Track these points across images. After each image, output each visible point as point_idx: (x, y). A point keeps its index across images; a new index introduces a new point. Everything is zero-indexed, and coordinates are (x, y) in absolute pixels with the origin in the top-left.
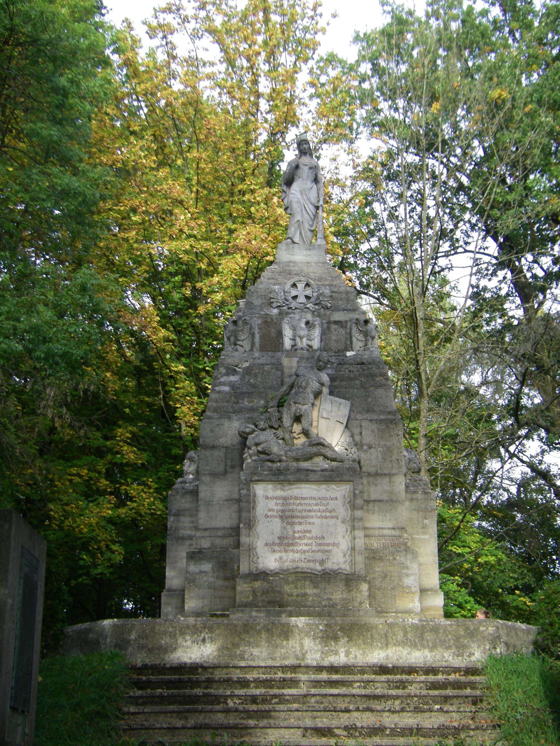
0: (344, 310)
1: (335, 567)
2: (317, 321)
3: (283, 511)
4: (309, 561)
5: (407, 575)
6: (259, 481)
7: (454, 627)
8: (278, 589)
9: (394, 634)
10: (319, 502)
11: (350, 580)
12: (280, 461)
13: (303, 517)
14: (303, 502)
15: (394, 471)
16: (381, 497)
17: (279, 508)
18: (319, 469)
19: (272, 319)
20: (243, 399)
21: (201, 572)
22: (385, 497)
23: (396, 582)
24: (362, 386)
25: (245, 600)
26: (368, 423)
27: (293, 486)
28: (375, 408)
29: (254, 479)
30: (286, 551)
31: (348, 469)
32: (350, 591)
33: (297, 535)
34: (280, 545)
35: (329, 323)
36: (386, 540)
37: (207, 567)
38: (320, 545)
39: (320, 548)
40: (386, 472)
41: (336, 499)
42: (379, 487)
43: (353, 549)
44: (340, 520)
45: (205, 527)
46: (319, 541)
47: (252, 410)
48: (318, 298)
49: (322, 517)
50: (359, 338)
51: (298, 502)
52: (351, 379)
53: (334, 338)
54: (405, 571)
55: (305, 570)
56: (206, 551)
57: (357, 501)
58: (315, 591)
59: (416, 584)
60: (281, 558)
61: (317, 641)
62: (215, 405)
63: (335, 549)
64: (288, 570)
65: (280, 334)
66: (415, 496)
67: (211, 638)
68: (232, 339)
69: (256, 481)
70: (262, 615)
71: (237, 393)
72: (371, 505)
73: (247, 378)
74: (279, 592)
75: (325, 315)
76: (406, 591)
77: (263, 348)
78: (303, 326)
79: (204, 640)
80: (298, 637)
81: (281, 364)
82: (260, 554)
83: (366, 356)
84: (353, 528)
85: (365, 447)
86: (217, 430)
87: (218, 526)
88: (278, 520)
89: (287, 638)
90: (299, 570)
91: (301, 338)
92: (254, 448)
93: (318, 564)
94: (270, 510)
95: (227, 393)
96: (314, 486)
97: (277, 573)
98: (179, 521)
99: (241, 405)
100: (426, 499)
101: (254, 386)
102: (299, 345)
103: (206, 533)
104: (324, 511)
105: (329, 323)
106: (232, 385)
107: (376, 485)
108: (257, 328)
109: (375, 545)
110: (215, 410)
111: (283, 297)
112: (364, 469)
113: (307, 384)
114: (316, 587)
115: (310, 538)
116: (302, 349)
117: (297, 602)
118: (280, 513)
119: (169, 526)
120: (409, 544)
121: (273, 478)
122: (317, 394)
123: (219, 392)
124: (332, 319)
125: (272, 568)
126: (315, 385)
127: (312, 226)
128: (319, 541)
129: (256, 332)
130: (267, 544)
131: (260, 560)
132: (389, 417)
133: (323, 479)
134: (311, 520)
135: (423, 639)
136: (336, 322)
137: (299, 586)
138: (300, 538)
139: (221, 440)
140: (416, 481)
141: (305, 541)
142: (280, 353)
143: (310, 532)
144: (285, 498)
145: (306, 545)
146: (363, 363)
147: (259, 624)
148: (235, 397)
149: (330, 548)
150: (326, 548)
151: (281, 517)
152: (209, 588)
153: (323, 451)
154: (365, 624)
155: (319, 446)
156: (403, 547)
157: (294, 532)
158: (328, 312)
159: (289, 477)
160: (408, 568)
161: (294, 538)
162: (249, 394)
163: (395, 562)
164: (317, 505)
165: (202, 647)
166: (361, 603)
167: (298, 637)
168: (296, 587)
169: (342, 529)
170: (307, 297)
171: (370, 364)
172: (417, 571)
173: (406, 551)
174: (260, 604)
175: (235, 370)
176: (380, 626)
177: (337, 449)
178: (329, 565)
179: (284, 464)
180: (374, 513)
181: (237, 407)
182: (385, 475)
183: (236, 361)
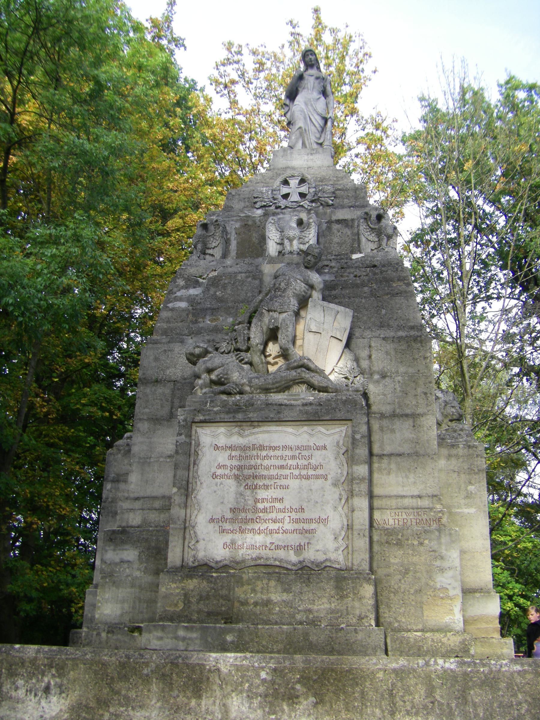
0: (350, 207)
1: (321, 557)
2: (313, 219)
3: (240, 468)
4: (278, 547)
5: (442, 570)
6: (205, 422)
7: (529, 676)
8: (224, 592)
9: (408, 691)
10: (297, 453)
11: (342, 579)
12: (241, 393)
13: (271, 477)
14: (272, 453)
15: (420, 411)
16: (400, 450)
17: (235, 463)
18: (299, 402)
19: (254, 222)
20: (204, 318)
21: (122, 561)
22: (406, 449)
23: (423, 580)
24: (373, 294)
25: (172, 609)
26: (380, 341)
27: (256, 430)
28: (391, 323)
29: (197, 419)
30: (242, 531)
31: (345, 402)
32: (342, 597)
33: (260, 506)
34: (233, 521)
35: (330, 222)
36: (408, 514)
37: (130, 554)
38: (298, 521)
39: (296, 526)
40: (408, 411)
41: (325, 448)
42: (398, 435)
43: (350, 527)
44: (329, 481)
45: (136, 495)
46: (294, 515)
47: (216, 330)
48: (315, 194)
49: (301, 477)
50: (370, 238)
51: (264, 453)
52: (356, 286)
53: (336, 240)
54: (438, 563)
55: (271, 562)
56: (131, 530)
57: (357, 451)
58: (285, 597)
59: (458, 585)
60: (233, 542)
61: (256, 702)
62: (165, 326)
63: (321, 528)
64: (244, 561)
65: (263, 239)
66: (454, 451)
67: (60, 686)
68: (199, 246)
69: (201, 422)
70: (194, 635)
71: (197, 310)
72: (385, 461)
73: (212, 290)
74: (227, 598)
75: (325, 213)
76: (442, 595)
77: (240, 255)
78: (294, 225)
79: (47, 690)
80: (218, 693)
81: (261, 271)
82: (201, 536)
83: (379, 257)
84: (351, 494)
85: (376, 377)
86: (163, 358)
87: (154, 494)
88: (231, 482)
89: (198, 694)
90: (262, 562)
91: (291, 240)
92: (204, 376)
93: (292, 552)
94: (219, 467)
95: (183, 310)
96: (290, 429)
97: (226, 566)
98: (117, 489)
99: (201, 325)
100: (470, 456)
101: (220, 300)
102: (288, 248)
103: (137, 505)
104: (305, 467)
105: (330, 222)
106: (191, 300)
107: (393, 431)
108: (234, 233)
109: (391, 522)
110: (165, 332)
111: (270, 196)
112: (374, 408)
113: (288, 284)
114: (287, 590)
115: (280, 511)
116: (291, 253)
117: (255, 614)
118: (235, 471)
119: (104, 496)
120: (444, 520)
121: (227, 417)
122: (303, 302)
123: (172, 310)
124: (334, 218)
125: (219, 558)
126: (300, 287)
127: (319, 139)
128: (294, 515)
129: (232, 238)
130: (212, 520)
131: (201, 545)
132: (412, 333)
133: (304, 417)
134: (284, 482)
135: (466, 703)
136: (338, 222)
137: (258, 588)
138: (265, 510)
139: (168, 372)
140: (455, 431)
141: (273, 515)
142: (260, 259)
143: (281, 500)
144: (244, 448)
145: (275, 521)
146: (375, 266)
147: (147, 664)
148: (194, 315)
149: (313, 526)
150: (306, 526)
151: (237, 477)
152: (133, 586)
153: (307, 375)
154: (350, 671)
155: (303, 372)
156: (436, 524)
157: (256, 501)
158: (329, 211)
159: (251, 415)
160: (442, 558)
161: (256, 510)
162: (214, 311)
163: (422, 549)
164: (293, 457)
165: (43, 703)
166: (360, 618)
167: (218, 693)
168: (254, 591)
169: (332, 494)
170: (302, 195)
171: (384, 266)
172: (457, 563)
173: (439, 531)
174: (195, 617)
175: (197, 281)
176: (380, 675)
177: (332, 377)
178: (311, 555)
179: (246, 397)
180: (389, 473)
181: (194, 327)
182: (407, 415)
183: (201, 271)
